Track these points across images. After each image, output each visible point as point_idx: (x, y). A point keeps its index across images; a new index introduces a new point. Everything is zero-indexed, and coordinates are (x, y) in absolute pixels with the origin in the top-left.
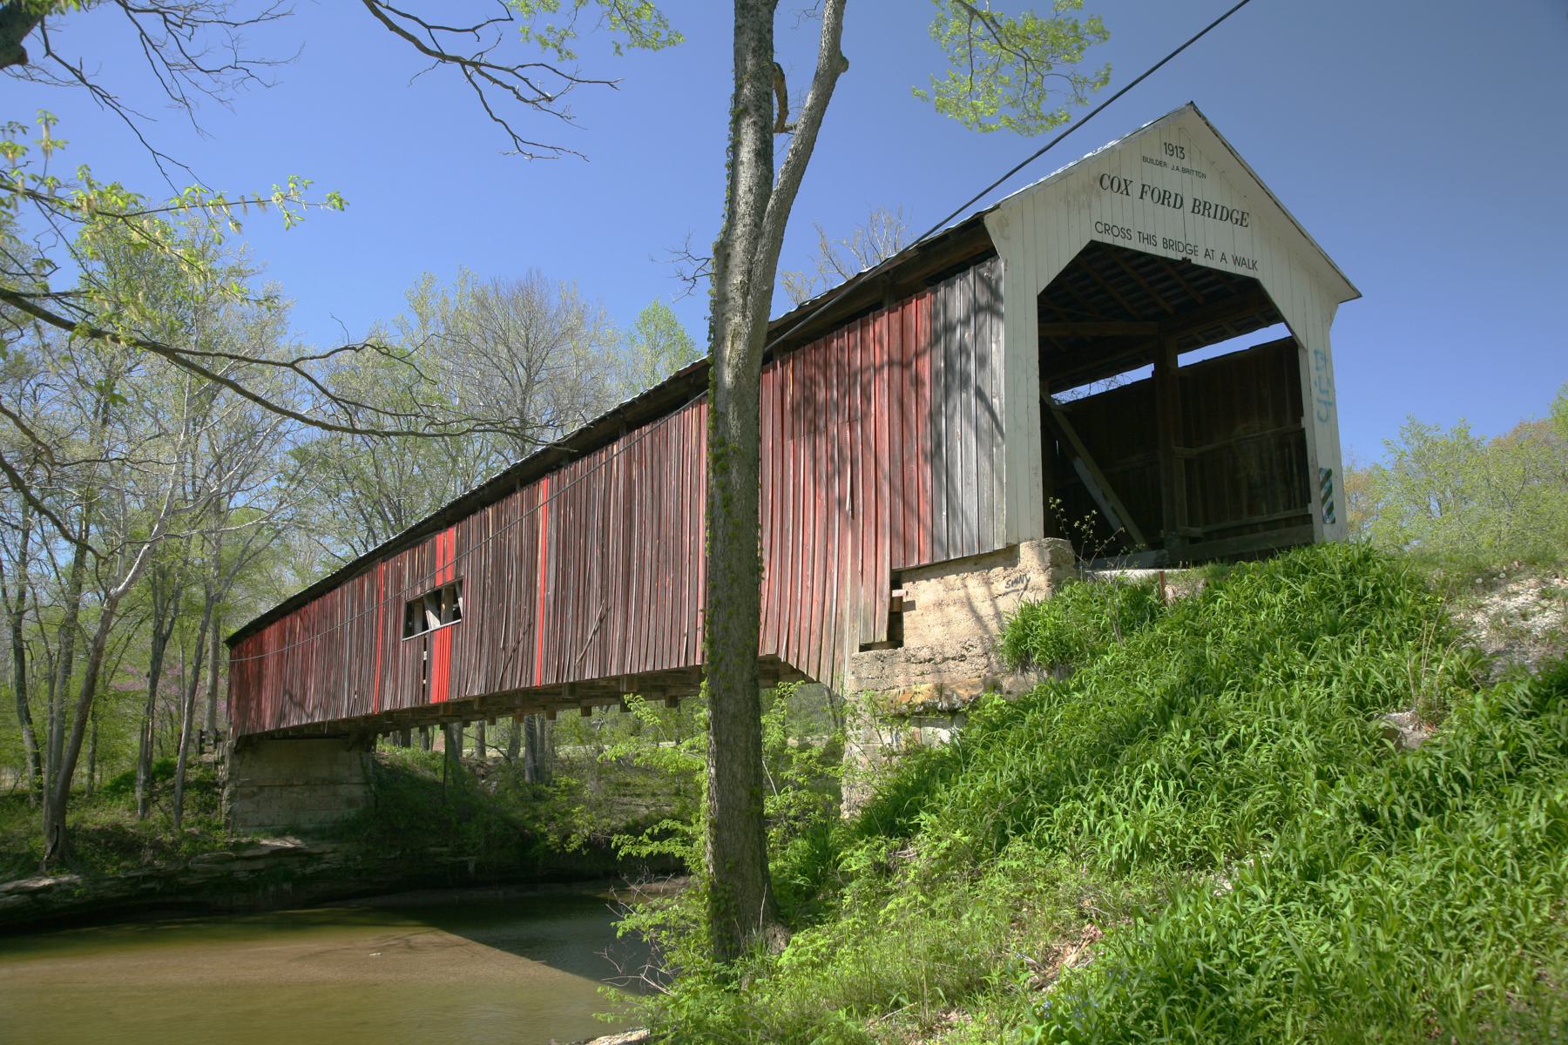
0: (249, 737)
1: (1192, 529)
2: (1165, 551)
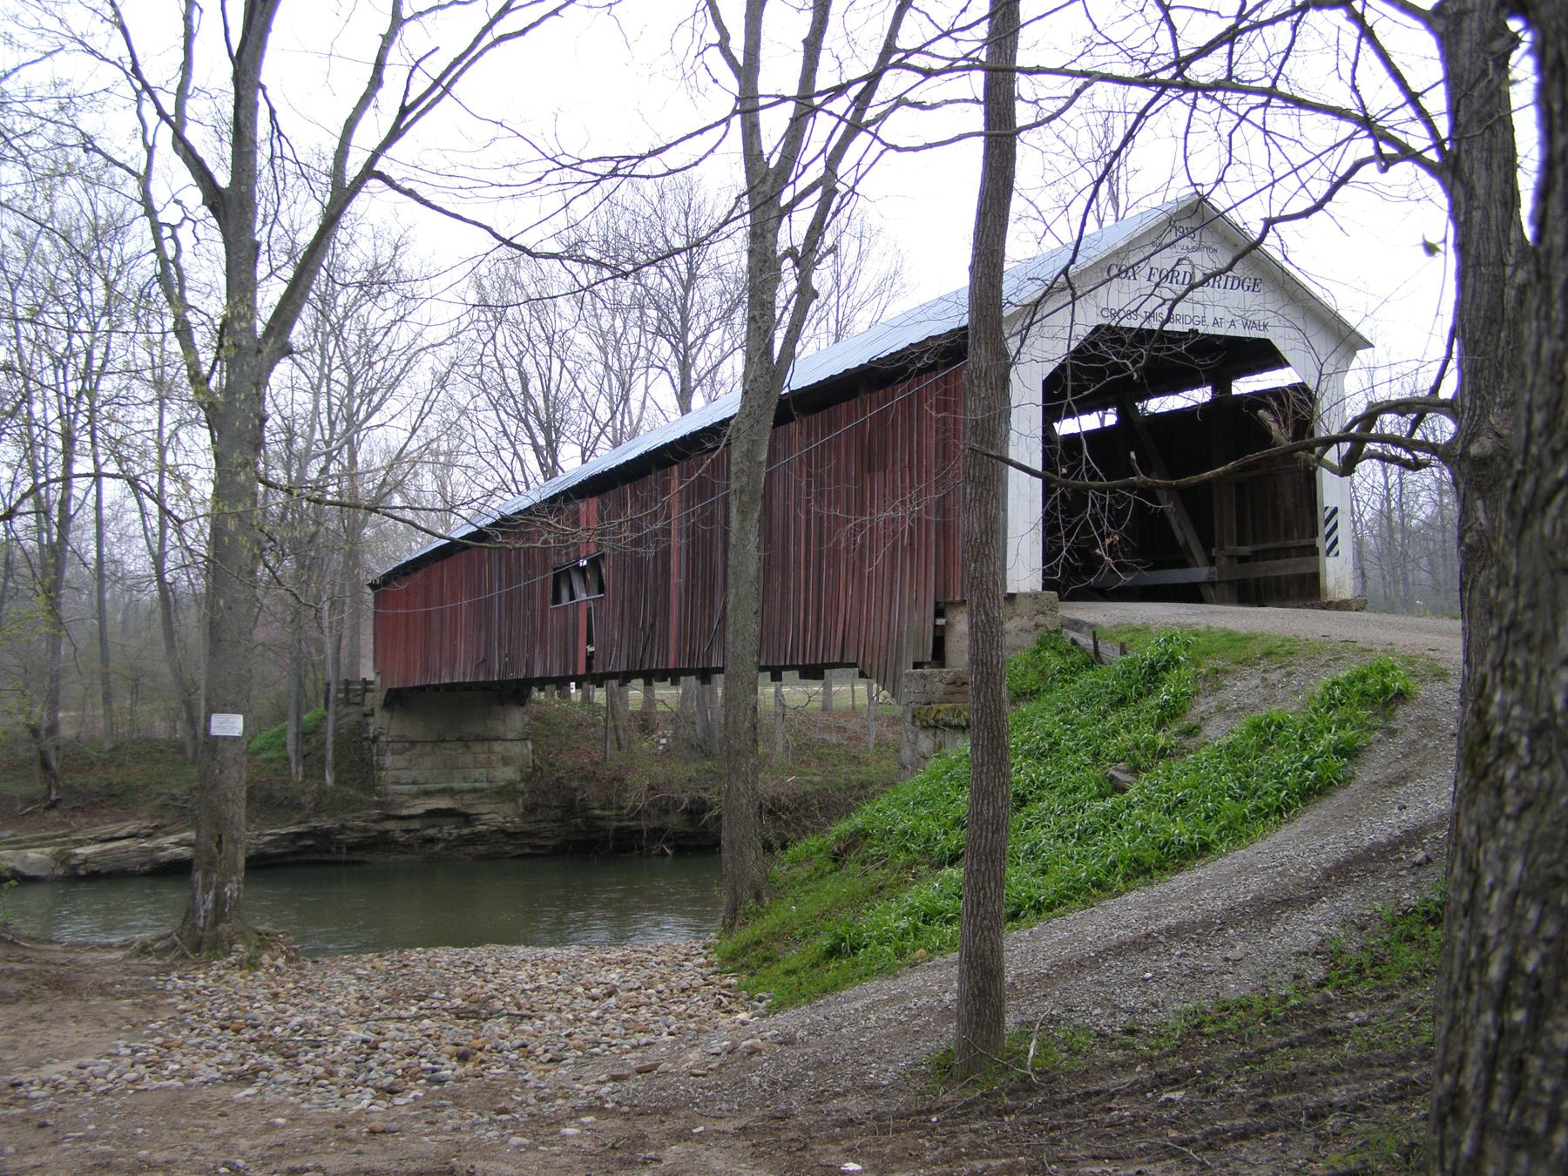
0: (398, 690)
1: (1241, 548)
2: (1214, 568)
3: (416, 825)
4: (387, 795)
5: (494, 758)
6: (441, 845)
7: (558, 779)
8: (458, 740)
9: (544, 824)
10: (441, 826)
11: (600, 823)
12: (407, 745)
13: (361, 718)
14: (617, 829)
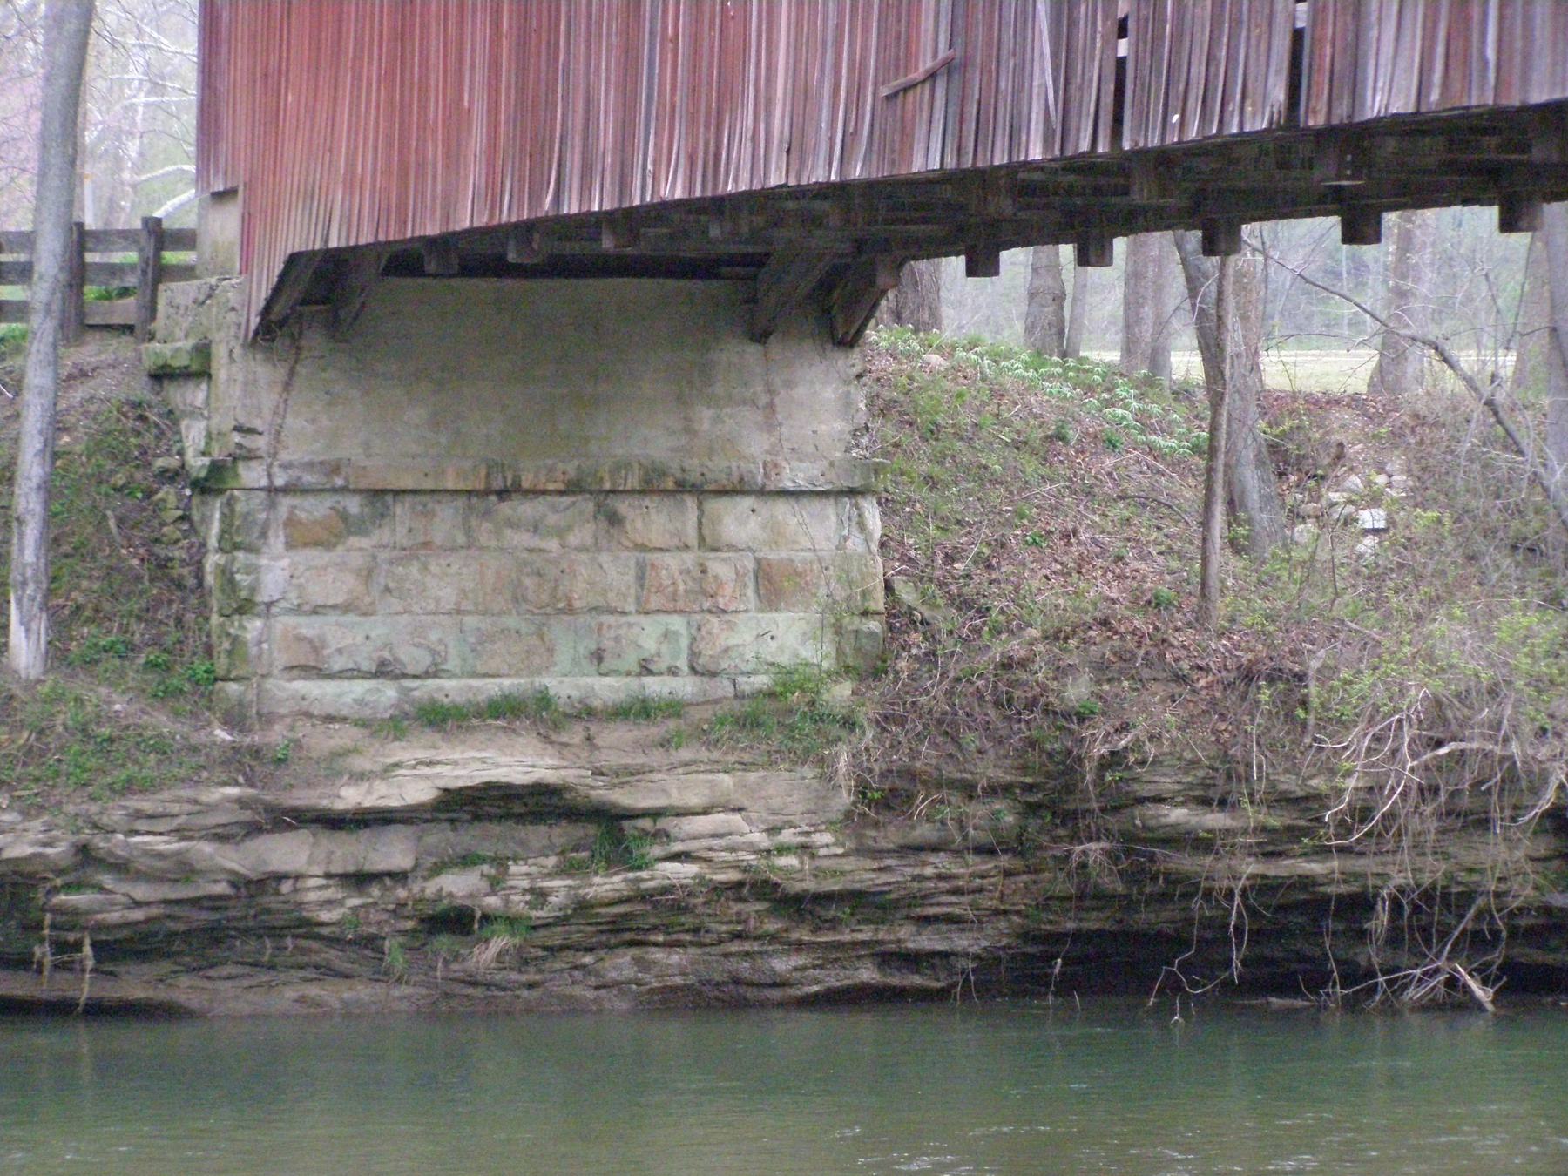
3: (393, 852)
4: (267, 719)
5: (720, 568)
6: (500, 942)
7: (1007, 664)
8: (573, 488)
9: (940, 862)
10: (500, 862)
11: (1185, 863)
12: (353, 505)
13: (141, 389)
14: (1264, 887)
